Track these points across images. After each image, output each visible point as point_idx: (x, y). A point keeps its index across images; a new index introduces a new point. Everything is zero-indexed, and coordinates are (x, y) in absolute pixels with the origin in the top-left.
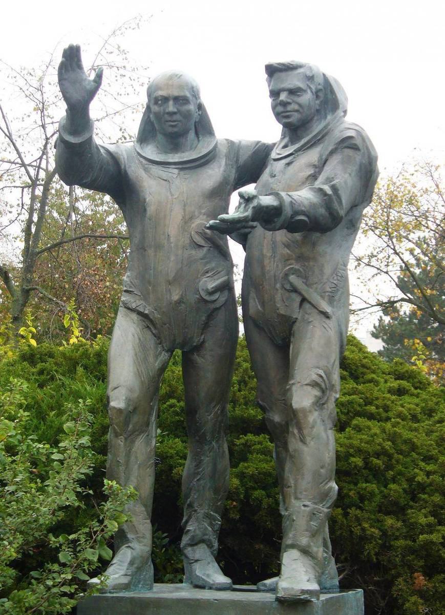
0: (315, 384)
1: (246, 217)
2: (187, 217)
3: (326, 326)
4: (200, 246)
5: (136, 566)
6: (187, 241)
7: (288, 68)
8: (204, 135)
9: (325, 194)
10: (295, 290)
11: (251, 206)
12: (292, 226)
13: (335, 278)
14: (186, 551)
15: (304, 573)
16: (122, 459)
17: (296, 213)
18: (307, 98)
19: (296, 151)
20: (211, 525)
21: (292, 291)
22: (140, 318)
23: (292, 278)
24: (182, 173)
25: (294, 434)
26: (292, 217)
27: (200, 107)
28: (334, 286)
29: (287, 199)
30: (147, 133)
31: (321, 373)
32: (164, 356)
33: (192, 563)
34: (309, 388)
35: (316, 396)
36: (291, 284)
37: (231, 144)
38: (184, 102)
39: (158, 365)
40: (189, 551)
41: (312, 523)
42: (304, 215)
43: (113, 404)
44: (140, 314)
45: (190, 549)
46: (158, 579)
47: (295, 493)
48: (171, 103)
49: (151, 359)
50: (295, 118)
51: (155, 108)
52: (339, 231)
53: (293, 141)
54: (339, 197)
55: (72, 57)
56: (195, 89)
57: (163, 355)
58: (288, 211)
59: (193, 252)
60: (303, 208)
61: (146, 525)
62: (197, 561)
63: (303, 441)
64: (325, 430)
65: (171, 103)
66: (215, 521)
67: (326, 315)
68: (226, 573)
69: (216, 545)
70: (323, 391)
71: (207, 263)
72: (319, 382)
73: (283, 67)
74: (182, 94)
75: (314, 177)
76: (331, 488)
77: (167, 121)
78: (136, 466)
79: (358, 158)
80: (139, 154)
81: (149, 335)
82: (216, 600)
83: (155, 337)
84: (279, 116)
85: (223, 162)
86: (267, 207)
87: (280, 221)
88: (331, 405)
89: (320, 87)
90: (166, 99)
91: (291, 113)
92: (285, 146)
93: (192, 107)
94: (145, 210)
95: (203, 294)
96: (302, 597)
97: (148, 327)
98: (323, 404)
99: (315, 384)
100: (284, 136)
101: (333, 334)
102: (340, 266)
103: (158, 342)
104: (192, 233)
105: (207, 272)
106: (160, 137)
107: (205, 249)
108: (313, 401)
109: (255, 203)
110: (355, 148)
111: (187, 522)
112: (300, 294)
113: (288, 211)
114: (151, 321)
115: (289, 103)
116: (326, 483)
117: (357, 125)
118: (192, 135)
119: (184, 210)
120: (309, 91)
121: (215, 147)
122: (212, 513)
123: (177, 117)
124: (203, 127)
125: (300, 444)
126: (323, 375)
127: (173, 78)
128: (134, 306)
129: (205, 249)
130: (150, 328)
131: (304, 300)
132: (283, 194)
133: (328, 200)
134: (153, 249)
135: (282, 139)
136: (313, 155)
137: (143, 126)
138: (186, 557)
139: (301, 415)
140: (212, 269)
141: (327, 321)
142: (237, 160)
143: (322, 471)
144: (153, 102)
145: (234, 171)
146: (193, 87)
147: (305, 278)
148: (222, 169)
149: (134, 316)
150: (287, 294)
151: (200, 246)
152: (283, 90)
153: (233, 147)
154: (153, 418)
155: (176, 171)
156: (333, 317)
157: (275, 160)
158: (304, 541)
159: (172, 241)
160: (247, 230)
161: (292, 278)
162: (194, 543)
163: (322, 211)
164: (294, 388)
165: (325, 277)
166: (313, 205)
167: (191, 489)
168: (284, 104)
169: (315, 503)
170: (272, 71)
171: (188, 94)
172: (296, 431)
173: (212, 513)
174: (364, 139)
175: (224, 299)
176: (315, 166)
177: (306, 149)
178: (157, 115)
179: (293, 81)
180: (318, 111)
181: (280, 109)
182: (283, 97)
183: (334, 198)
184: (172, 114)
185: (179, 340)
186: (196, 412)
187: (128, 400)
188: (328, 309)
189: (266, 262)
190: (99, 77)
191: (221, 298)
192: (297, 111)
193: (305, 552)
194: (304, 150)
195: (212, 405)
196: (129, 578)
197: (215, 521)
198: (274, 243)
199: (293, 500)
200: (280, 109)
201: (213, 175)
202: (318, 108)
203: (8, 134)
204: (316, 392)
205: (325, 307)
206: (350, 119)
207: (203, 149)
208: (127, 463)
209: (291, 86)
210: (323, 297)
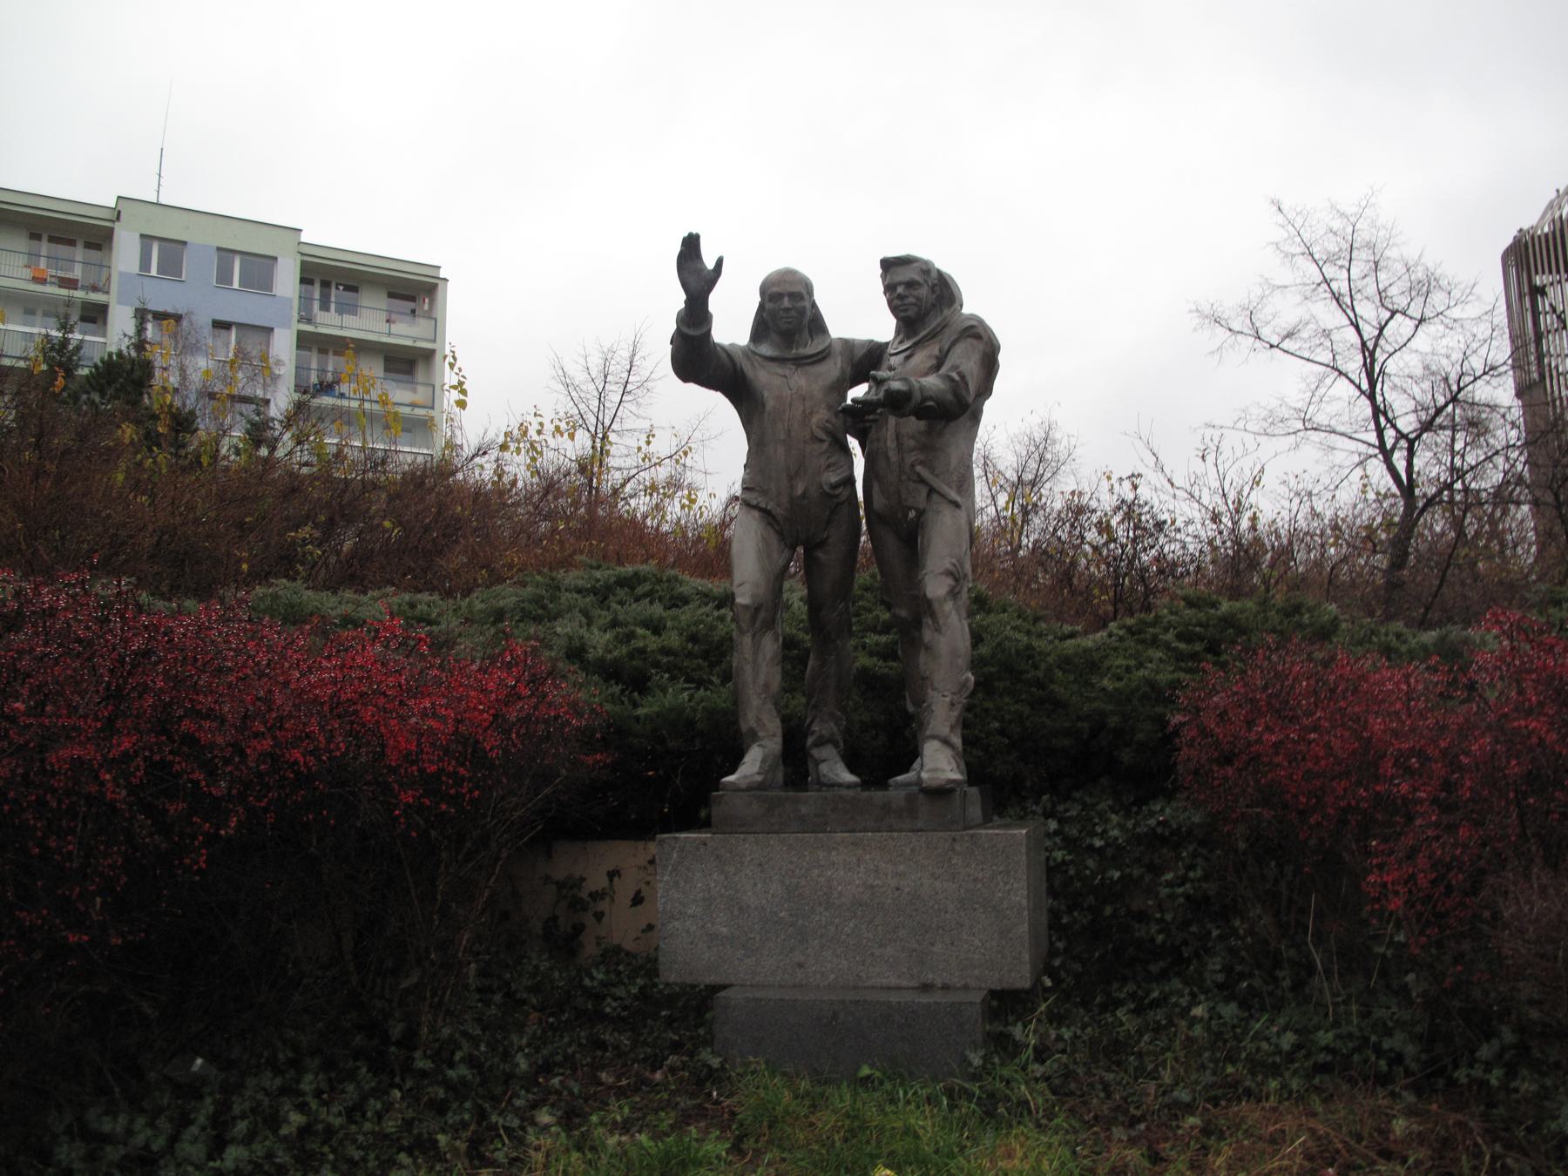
0: (949, 573)
1: (879, 400)
4: (822, 441)
9: (952, 380)
10: (922, 481)
11: (883, 388)
12: (921, 412)
16: (748, 654)
17: (925, 399)
18: (923, 292)
19: (915, 344)
20: (837, 724)
23: (919, 468)
27: (814, 305)
29: (916, 385)
30: (761, 328)
31: (954, 561)
32: (787, 553)
34: (943, 577)
36: (919, 475)
40: (815, 752)
43: (739, 600)
48: (786, 299)
51: (769, 306)
52: (964, 419)
53: (908, 337)
54: (966, 384)
55: (691, 246)
58: (917, 396)
62: (823, 761)
64: (960, 620)
65: (786, 299)
67: (957, 505)
68: (852, 771)
69: (842, 744)
70: (957, 580)
75: (938, 367)
76: (967, 680)
84: (894, 309)
85: (839, 359)
88: (964, 595)
90: (779, 296)
92: (901, 342)
94: (764, 405)
95: (826, 488)
99: (949, 573)
100: (898, 332)
101: (963, 521)
106: (774, 336)
110: (978, 337)
111: (812, 722)
113: (917, 396)
114: (773, 517)
118: (806, 333)
121: (830, 345)
122: (547, 791)
123: (793, 313)
124: (817, 325)
128: (755, 503)
131: (932, 490)
132: (912, 379)
135: (895, 337)
136: (934, 349)
138: (812, 756)
139: (936, 606)
144: (767, 298)
145: (849, 369)
147: (932, 469)
149: (756, 514)
151: (822, 441)
152: (900, 283)
153: (848, 344)
158: (945, 731)
161: (919, 468)
162: (820, 743)
163: (950, 397)
164: (927, 578)
168: (900, 297)
170: (888, 265)
171: (804, 292)
172: (930, 622)
173: (547, 791)
176: (937, 358)
178: (773, 314)
180: (934, 305)
181: (897, 302)
182: (900, 290)
184: (787, 310)
187: (753, 596)
188: (959, 499)
190: (720, 262)
191: (845, 494)
193: (946, 742)
199: (930, 691)
200: (897, 302)
201: (832, 369)
204: (950, 581)
205: (953, 495)
206: (966, 310)
207: (811, 349)
208: (755, 661)
210: (950, 487)
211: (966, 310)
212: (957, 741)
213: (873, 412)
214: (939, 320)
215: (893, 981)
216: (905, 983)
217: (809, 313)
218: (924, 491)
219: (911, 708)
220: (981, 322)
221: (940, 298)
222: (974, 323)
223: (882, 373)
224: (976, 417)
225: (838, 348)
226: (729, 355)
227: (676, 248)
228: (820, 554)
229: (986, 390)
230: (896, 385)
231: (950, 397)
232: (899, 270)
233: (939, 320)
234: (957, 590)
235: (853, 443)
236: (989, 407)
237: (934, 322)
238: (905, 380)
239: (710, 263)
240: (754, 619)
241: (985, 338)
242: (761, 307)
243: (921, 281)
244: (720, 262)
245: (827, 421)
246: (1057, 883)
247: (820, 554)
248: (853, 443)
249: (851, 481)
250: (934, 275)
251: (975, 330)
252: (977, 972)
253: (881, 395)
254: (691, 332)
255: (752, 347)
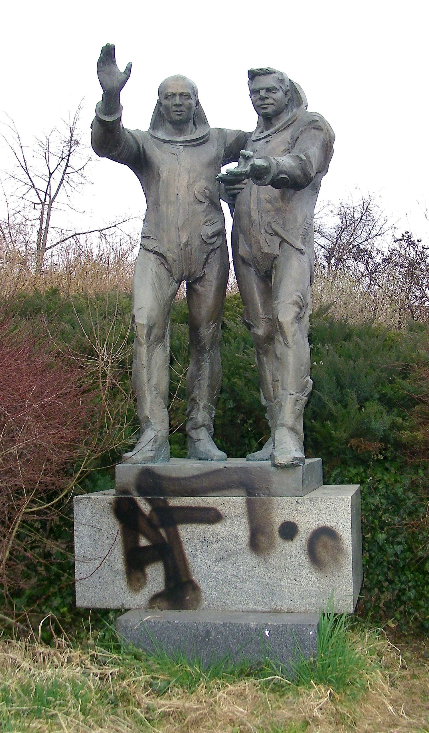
0: (296, 303)
2: (191, 181)
3: (301, 260)
5: (158, 443)
6: (192, 199)
7: (267, 72)
8: (200, 125)
10: (276, 234)
13: (306, 225)
14: (190, 434)
15: (292, 445)
17: (281, 172)
18: (279, 95)
21: (274, 235)
22: (156, 256)
24: (186, 149)
25: (280, 342)
26: (278, 174)
27: (197, 103)
28: (306, 231)
31: (299, 294)
32: (175, 285)
33: (196, 442)
35: (296, 312)
37: (220, 130)
38: (187, 97)
39: (170, 292)
41: (296, 407)
42: (286, 174)
44: (156, 253)
45: (193, 431)
46: (173, 455)
47: (282, 385)
49: (165, 287)
50: (270, 110)
54: (310, 163)
56: (194, 89)
57: (173, 284)
58: (274, 170)
59: (197, 207)
60: (285, 169)
61: (164, 412)
63: (287, 345)
64: (303, 338)
65: (178, 97)
66: (212, 411)
70: (301, 308)
71: (207, 215)
72: (299, 301)
73: (262, 72)
74: (186, 91)
77: (174, 111)
78: (156, 369)
79: (321, 135)
80: (152, 136)
81: (163, 270)
82: (225, 467)
83: (168, 271)
84: (257, 108)
86: (259, 166)
87: (268, 178)
89: (288, 88)
91: (268, 106)
93: (193, 102)
96: (294, 463)
97: (162, 263)
98: (301, 318)
102: (308, 217)
103: (170, 275)
104: (196, 192)
105: (207, 222)
106: (168, 125)
107: (205, 205)
108: (294, 315)
109: (251, 162)
110: (319, 129)
112: (280, 236)
115: (267, 98)
116: (305, 378)
117: (319, 114)
118: (191, 123)
119: (189, 175)
120: (281, 91)
121: (209, 132)
125: (285, 348)
126: (301, 296)
127: (179, 79)
129: (205, 205)
130: (164, 265)
133: (304, 165)
134: (165, 205)
136: (286, 135)
137: (154, 118)
140: (210, 220)
141: (302, 256)
142: (225, 143)
143: (302, 368)
144: (163, 97)
146: (193, 87)
148: (216, 148)
149: (152, 256)
150: (270, 237)
154: (167, 333)
155: (182, 148)
156: (306, 253)
157: (254, 141)
159: (180, 198)
160: (236, 191)
163: (298, 172)
165: (298, 224)
166: (291, 167)
167: (194, 387)
168: (262, 99)
169: (298, 393)
170: (253, 75)
172: (281, 339)
174: (325, 123)
175: (220, 242)
177: (281, 131)
179: (268, 82)
183: (308, 163)
185: (186, 274)
186: (198, 329)
187: (149, 317)
188: (303, 248)
189: (253, 214)
190: (129, 69)
192: (272, 104)
193: (293, 429)
194: (278, 132)
195: (211, 323)
196: (154, 452)
197: (212, 411)
198: (259, 199)
200: (259, 102)
202: (287, 103)
203: (24, 165)
205: (299, 245)
206: (309, 110)
208: (149, 367)
209: (269, 86)
211: (309, 110)
212: (300, 428)
213: (239, 182)
214: (290, 115)
215: (251, 606)
216: (260, 608)
217: (194, 109)
218: (277, 240)
219: (264, 402)
220: (322, 118)
221: (291, 100)
222: (317, 119)
223: (248, 152)
224: (316, 189)
225: (214, 135)
226: (134, 138)
227: (97, 55)
228: (198, 286)
229: (323, 169)
230: (259, 162)
231: (298, 172)
232: (261, 78)
233: (290, 115)
234: (301, 316)
235: (225, 206)
236: (326, 181)
237: (285, 118)
238: (265, 158)
239: (121, 66)
240: (149, 335)
241: (325, 130)
242: (159, 103)
243: (278, 87)
244: (129, 69)
245: (206, 189)
246: (29, 601)
247: (198, 286)
248: (225, 206)
249: (222, 233)
250: (287, 83)
251: (318, 124)
252: (313, 600)
253: (248, 168)
254: (107, 119)
255: (151, 131)
